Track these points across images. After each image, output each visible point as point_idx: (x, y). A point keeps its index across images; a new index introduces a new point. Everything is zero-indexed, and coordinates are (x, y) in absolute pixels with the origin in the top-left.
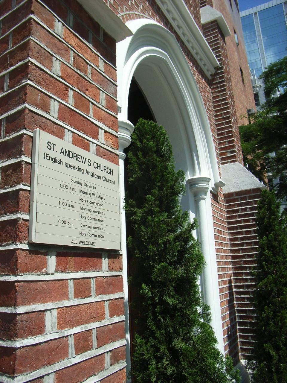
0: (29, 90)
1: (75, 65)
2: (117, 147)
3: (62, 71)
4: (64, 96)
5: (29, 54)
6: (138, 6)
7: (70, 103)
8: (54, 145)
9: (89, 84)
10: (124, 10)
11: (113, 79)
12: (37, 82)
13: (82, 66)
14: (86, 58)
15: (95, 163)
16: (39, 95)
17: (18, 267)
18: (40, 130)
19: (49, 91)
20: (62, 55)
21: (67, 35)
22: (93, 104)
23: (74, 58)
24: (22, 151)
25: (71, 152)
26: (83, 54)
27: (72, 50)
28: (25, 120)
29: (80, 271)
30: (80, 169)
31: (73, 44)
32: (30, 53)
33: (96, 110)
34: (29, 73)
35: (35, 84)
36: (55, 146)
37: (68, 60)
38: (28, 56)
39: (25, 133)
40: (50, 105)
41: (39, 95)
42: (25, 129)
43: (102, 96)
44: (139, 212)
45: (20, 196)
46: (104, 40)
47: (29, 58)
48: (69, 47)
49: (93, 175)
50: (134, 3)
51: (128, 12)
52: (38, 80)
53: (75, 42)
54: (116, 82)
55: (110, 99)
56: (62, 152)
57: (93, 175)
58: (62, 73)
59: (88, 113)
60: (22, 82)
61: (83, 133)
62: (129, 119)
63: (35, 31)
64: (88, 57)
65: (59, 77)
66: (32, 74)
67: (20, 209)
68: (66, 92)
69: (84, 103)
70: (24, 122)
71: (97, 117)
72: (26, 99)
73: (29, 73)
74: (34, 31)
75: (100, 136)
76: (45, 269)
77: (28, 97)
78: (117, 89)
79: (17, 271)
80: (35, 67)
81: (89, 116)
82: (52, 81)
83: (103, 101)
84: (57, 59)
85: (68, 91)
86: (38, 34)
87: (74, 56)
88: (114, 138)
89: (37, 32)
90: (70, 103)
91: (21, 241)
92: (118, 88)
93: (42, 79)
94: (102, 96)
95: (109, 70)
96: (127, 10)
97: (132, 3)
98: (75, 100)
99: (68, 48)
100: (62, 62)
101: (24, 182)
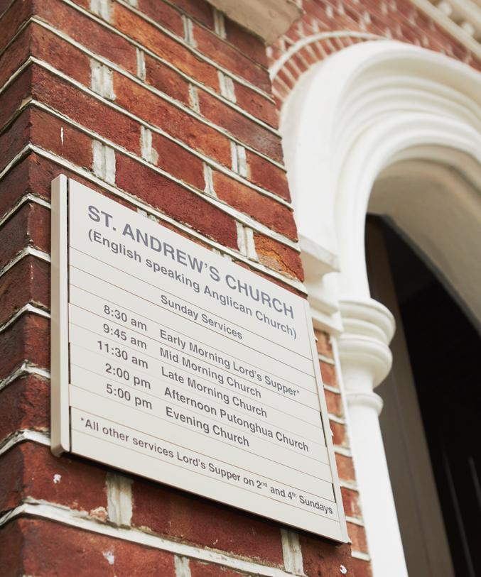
0: (35, 119)
1: (151, 81)
2: (299, 275)
3: (118, 89)
4: (130, 136)
5: (29, 51)
6: (355, 18)
7: (148, 155)
8: (107, 216)
9: (196, 125)
10: (316, 29)
11: (267, 122)
12: (53, 104)
13: (171, 84)
14: (180, 70)
15: (278, 434)
16: (62, 129)
17: (25, 483)
18: (70, 180)
19: (88, 126)
20: (114, 59)
21: (122, 19)
22: (213, 168)
23: (147, 67)
24: (27, 237)
25: (154, 240)
26: (171, 60)
27: (140, 50)
28: (30, 175)
29: (211, 547)
30: (230, 437)
31: (142, 39)
32: (34, 49)
33: (222, 183)
34: (33, 86)
35: (50, 108)
36: (109, 218)
37: (133, 69)
38: (29, 54)
39: (32, 199)
40: (92, 155)
41: (62, 129)
42: (31, 193)
43: (238, 153)
44: (291, 221)
45: (24, 328)
46: (227, 37)
47: (31, 57)
48: (131, 43)
49: (225, 300)
50: (341, 11)
51: (327, 35)
52: (57, 101)
53: (146, 36)
54: (277, 129)
55: (263, 164)
56: (128, 231)
57: (225, 300)
58: (118, 93)
59: (201, 185)
60: (37, 428)
61: (191, 226)
62: (373, 296)
63: (43, 7)
64: (187, 68)
65: (110, 101)
66: (40, 89)
67: (28, 356)
68: (134, 134)
69: (185, 162)
70: (29, 178)
71: (229, 198)
72: (29, 134)
73: (33, 86)
74: (38, 8)
75: (240, 241)
76: (101, 509)
77: (34, 131)
78: (280, 145)
79: (23, 491)
80: (46, 76)
81: (203, 193)
82: (93, 107)
83: (240, 168)
84: (102, 64)
85: (138, 132)
86: (48, 13)
87: (146, 62)
88: (285, 254)
89: (45, 10)
90: (148, 155)
91: (32, 424)
92: (283, 142)
93: (68, 100)
94: (238, 153)
95: (253, 101)
96: (322, 29)
97: (336, 13)
98: (161, 154)
99: (128, 45)
100: (114, 70)
101: (34, 300)
